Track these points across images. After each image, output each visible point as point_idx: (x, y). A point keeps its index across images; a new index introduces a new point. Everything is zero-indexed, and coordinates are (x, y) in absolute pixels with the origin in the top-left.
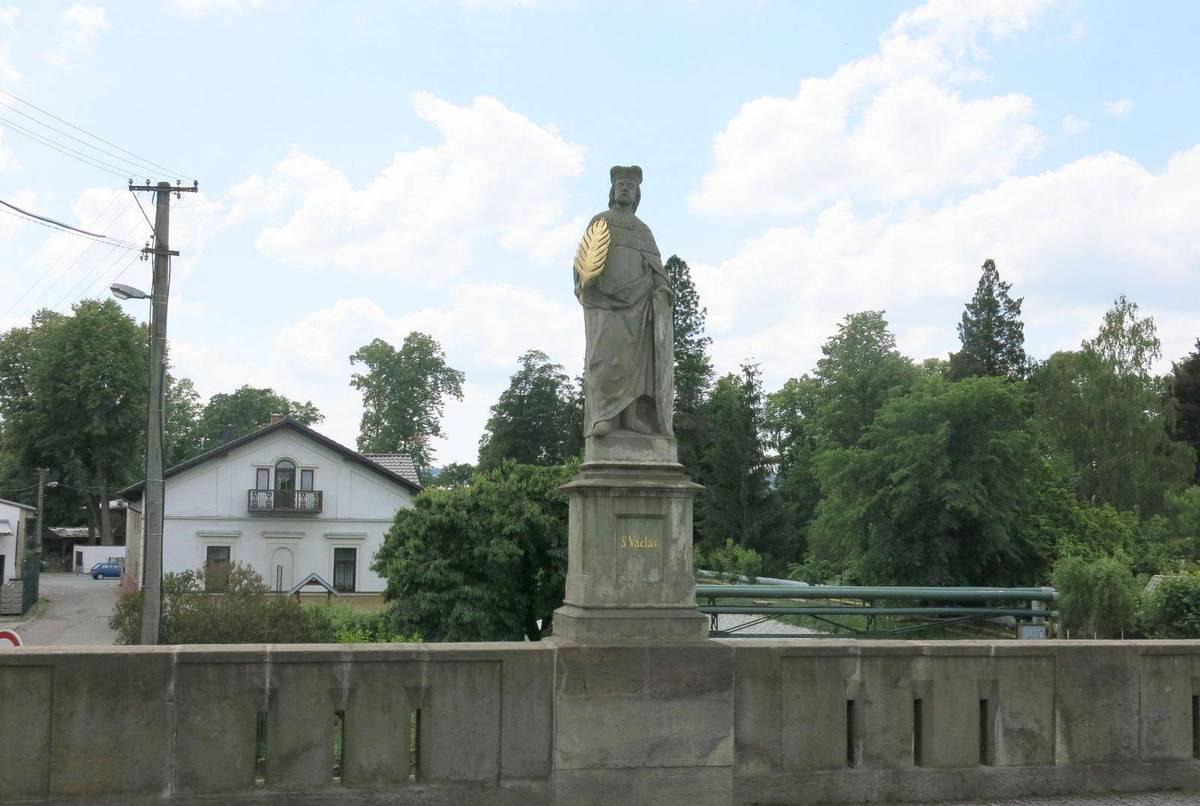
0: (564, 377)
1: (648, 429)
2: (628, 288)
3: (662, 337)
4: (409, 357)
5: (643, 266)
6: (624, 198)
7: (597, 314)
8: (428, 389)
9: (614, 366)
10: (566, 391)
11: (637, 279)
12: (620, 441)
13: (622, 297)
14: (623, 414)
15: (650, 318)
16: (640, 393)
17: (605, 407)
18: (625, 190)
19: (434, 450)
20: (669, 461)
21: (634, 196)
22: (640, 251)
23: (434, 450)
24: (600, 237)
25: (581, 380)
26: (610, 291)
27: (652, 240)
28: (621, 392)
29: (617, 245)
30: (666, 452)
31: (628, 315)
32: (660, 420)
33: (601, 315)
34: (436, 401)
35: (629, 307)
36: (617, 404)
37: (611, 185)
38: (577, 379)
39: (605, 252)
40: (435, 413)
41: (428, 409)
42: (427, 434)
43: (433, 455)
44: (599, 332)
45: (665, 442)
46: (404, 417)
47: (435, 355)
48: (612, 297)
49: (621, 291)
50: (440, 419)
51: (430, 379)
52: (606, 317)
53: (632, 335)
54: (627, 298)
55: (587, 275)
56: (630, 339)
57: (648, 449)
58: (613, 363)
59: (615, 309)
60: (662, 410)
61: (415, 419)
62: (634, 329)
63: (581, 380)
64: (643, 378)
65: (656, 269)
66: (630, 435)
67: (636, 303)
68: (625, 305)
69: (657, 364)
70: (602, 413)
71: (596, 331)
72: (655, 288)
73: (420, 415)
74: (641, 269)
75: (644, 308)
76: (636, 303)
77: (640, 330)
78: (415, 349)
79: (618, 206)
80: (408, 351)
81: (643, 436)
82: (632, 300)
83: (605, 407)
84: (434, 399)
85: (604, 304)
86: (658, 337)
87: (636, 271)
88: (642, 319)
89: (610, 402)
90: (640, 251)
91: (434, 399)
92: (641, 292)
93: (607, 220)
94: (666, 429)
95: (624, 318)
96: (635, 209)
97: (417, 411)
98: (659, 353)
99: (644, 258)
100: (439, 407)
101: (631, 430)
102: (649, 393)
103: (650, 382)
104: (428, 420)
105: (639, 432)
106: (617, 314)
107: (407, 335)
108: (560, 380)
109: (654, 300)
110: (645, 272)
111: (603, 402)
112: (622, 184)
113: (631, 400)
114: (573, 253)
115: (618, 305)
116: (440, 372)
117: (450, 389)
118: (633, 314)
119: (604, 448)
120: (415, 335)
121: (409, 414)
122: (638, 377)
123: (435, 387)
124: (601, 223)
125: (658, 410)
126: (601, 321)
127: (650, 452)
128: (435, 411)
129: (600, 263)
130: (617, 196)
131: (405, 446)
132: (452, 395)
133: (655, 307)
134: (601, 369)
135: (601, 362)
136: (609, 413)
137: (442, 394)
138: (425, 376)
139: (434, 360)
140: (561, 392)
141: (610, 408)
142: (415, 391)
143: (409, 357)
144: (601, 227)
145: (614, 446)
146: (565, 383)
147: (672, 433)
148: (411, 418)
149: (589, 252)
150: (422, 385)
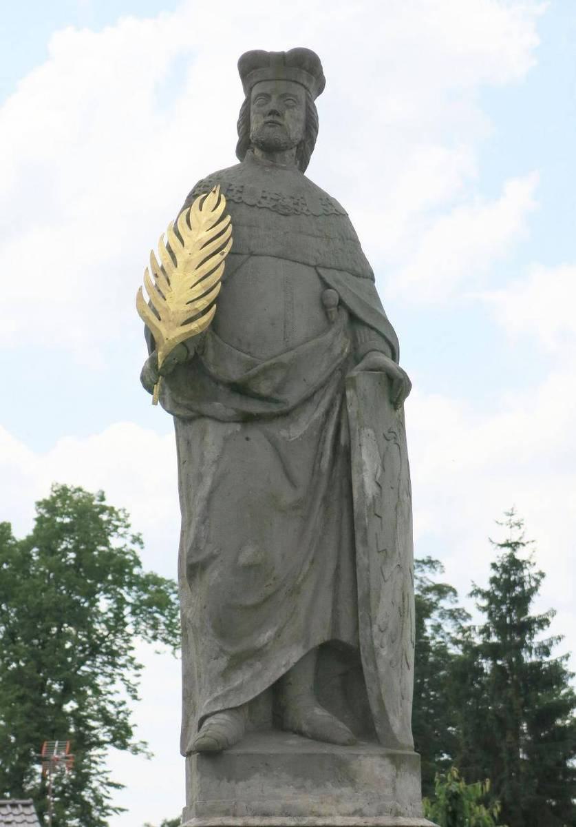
0: (442, 590)
1: (342, 729)
2: (281, 365)
3: (370, 489)
4: (49, 550)
5: (325, 307)
6: (274, 134)
7: (204, 432)
8: (101, 629)
9: (249, 567)
10: (449, 626)
11: (307, 340)
12: (265, 764)
13: (264, 388)
14: (278, 689)
15: (343, 441)
16: (320, 636)
17: (225, 675)
18: (272, 113)
19: (117, 786)
20: (398, 814)
21: (300, 126)
22: (315, 267)
23: (117, 786)
24: (206, 235)
25: (486, 595)
26: (234, 372)
27: (350, 240)
28: (270, 633)
29: (252, 254)
30: (388, 791)
31: (284, 433)
32: (375, 709)
33: (213, 436)
34: (121, 661)
35: (285, 414)
36: (258, 665)
37: (241, 97)
38: (477, 592)
39: (219, 273)
40: (117, 691)
41: (100, 680)
42: (100, 744)
43: (114, 798)
44: (208, 482)
45: (386, 762)
46: (40, 703)
47: (115, 542)
48: (240, 389)
49: (265, 371)
50: (131, 704)
51: (104, 604)
52: (226, 440)
53: (293, 484)
54: (278, 390)
55: (172, 334)
56: (288, 497)
57: (340, 783)
58: (243, 560)
59: (247, 419)
60: (377, 680)
61: (70, 706)
62: (301, 474)
63: (486, 595)
64: (325, 600)
65: (360, 313)
66: (292, 745)
67: (307, 400)
68: (275, 409)
69: (362, 559)
70: (220, 691)
71: (200, 477)
72: (357, 362)
73: (80, 698)
74: (318, 314)
75: (328, 413)
76: (307, 400)
77: (315, 471)
78: (66, 529)
79: (258, 153)
80: (47, 534)
81: (327, 749)
82: (292, 396)
83: (225, 675)
84: (114, 654)
85: (218, 407)
86: (362, 486)
87: (305, 319)
88: (321, 440)
89: (237, 662)
90: (315, 267)
91: (114, 654)
92: (316, 373)
93: (227, 190)
94: (389, 729)
95: (274, 444)
96: (303, 162)
97: (73, 688)
98: (365, 530)
99: (327, 286)
100: (129, 673)
101: (301, 733)
102: (345, 636)
103: (346, 608)
104: (102, 711)
105: (318, 737)
106: (256, 434)
107: (47, 495)
108: (432, 597)
109: (349, 394)
110: (330, 322)
111: (223, 662)
112: (267, 97)
113: (295, 654)
114: (137, 278)
115: (256, 407)
116: (130, 585)
117: (154, 627)
118: (296, 431)
119: (225, 783)
120: (63, 493)
121: (52, 694)
122: (316, 593)
123: (117, 624)
124: (212, 199)
125: (369, 683)
126: (212, 451)
127: (347, 790)
128: (119, 685)
129: (202, 304)
130: (254, 127)
131: (44, 778)
132: (159, 644)
133: (351, 410)
134: (213, 575)
135: (213, 557)
136: (239, 689)
137: (136, 641)
138: (91, 595)
139: (111, 555)
140: (437, 628)
141: (239, 678)
142: (68, 636)
143: (49, 550)
144: (212, 208)
145: (245, 777)
146: (446, 604)
147: (408, 738)
148: (59, 706)
149: (175, 275)
150: (82, 619)
